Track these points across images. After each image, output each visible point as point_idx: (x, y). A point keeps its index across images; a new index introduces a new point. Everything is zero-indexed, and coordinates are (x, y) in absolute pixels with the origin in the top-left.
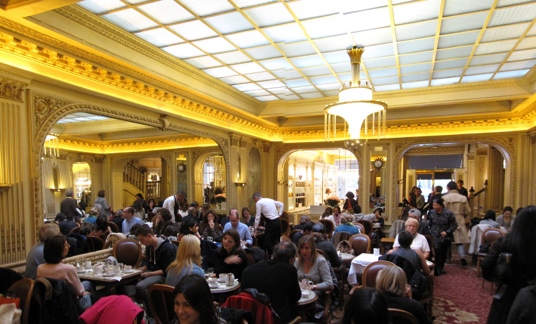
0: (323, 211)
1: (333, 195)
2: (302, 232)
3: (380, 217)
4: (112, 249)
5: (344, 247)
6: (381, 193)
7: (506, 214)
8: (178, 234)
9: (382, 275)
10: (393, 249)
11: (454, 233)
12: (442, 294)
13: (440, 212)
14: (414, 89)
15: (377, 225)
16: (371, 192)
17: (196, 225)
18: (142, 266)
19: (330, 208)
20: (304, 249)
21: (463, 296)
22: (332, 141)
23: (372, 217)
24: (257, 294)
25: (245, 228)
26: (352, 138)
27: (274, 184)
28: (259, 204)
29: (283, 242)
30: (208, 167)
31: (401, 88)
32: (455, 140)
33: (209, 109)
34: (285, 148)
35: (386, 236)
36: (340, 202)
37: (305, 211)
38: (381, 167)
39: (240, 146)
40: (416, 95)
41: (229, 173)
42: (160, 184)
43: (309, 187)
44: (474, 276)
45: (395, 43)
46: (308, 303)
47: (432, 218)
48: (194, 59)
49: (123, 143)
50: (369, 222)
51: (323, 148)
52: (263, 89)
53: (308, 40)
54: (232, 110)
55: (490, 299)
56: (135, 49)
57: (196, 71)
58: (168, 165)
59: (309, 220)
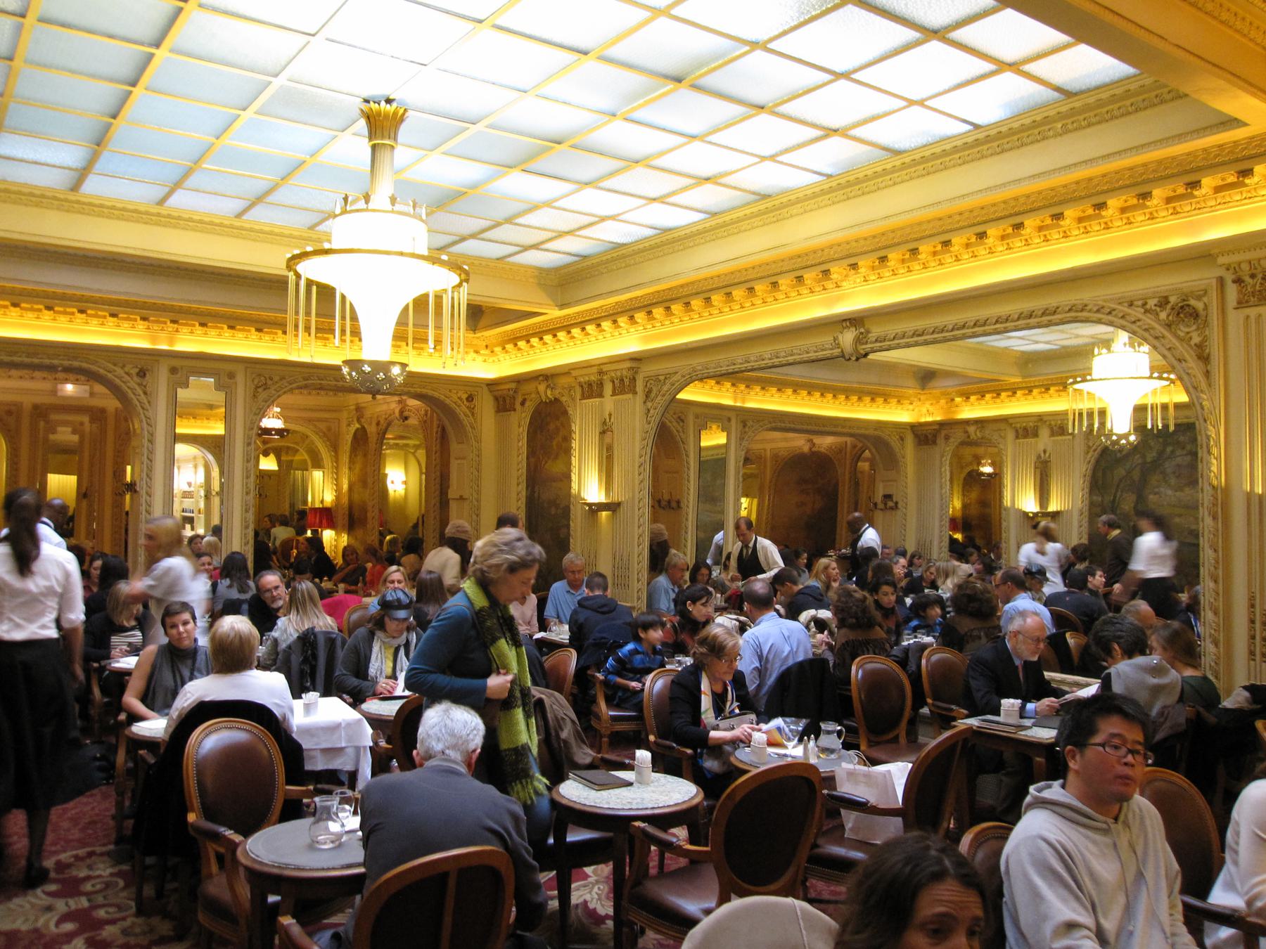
34: (282, 378)
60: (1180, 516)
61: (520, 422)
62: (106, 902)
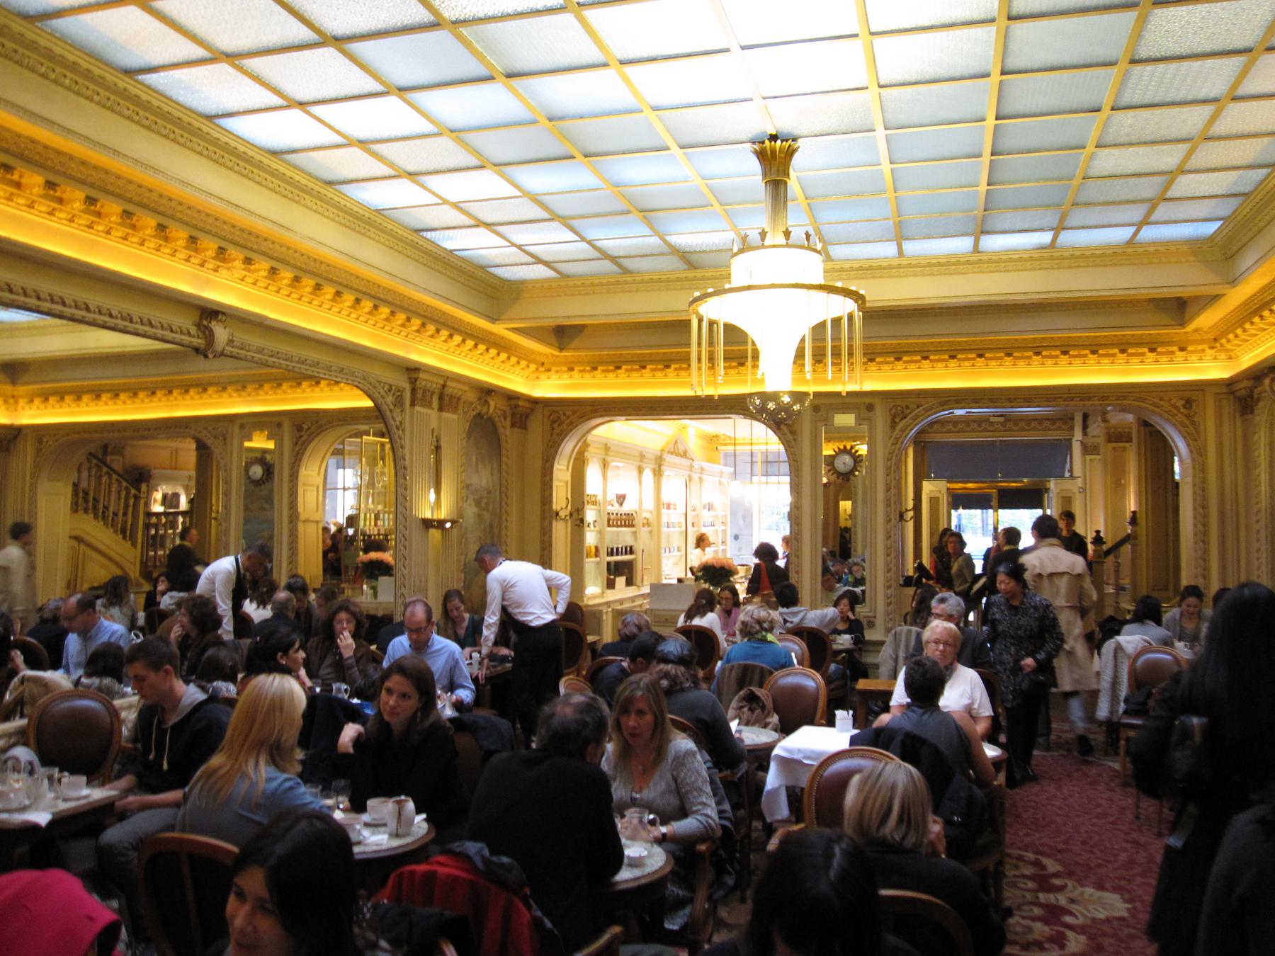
0: (687, 602)
1: (716, 552)
2: (625, 664)
3: (852, 617)
4: (24, 722)
5: (750, 709)
6: (853, 546)
7: (1189, 606)
8: (240, 676)
9: (860, 790)
10: (892, 710)
11: (1056, 662)
12: (1028, 840)
13: (1016, 603)
14: (936, 257)
15: (845, 641)
16: (825, 545)
17: (297, 645)
18: (119, 776)
19: (708, 590)
20: (633, 716)
21: (1084, 843)
22: (712, 396)
23: (828, 618)
24: (484, 860)
25: (452, 654)
26: (769, 387)
27: (543, 518)
28: (497, 580)
29: (568, 696)
30: (341, 471)
31: (901, 253)
32: (1048, 401)
33: (349, 298)
34: (574, 413)
35: (870, 671)
36: (737, 573)
37: (633, 601)
38: (851, 472)
39: (441, 409)
40: (940, 274)
41: (406, 489)
42: (187, 519)
43: (647, 529)
44: (1113, 785)
45: (881, 133)
46: (643, 881)
47: (995, 620)
48: (311, 153)
49: (78, 394)
50: (822, 632)
51: (650, 415)
52: (513, 245)
53: (642, 111)
54: (419, 302)
55: (1156, 850)
56: (136, 118)
57: (317, 188)
58: (218, 462)
59: (648, 627)
62: (1025, 893)
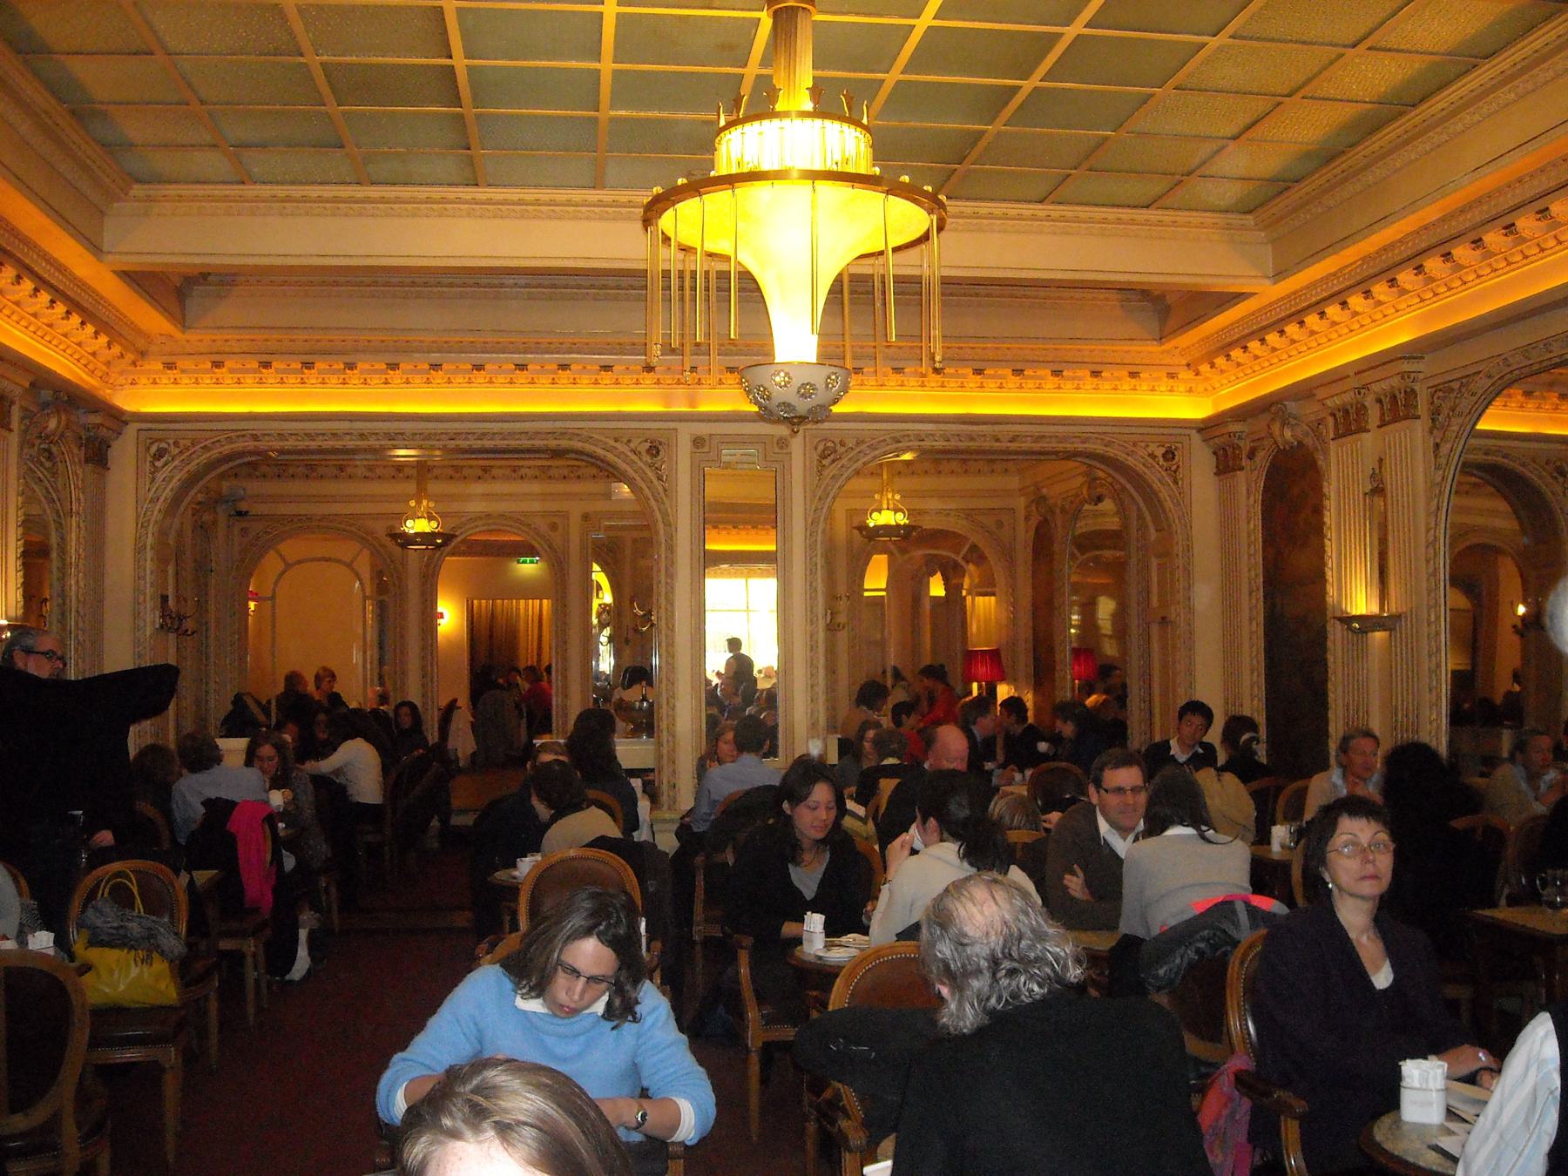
60: (933, 359)
61: (1249, 487)
